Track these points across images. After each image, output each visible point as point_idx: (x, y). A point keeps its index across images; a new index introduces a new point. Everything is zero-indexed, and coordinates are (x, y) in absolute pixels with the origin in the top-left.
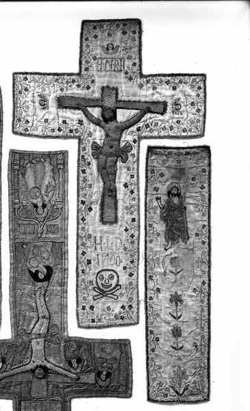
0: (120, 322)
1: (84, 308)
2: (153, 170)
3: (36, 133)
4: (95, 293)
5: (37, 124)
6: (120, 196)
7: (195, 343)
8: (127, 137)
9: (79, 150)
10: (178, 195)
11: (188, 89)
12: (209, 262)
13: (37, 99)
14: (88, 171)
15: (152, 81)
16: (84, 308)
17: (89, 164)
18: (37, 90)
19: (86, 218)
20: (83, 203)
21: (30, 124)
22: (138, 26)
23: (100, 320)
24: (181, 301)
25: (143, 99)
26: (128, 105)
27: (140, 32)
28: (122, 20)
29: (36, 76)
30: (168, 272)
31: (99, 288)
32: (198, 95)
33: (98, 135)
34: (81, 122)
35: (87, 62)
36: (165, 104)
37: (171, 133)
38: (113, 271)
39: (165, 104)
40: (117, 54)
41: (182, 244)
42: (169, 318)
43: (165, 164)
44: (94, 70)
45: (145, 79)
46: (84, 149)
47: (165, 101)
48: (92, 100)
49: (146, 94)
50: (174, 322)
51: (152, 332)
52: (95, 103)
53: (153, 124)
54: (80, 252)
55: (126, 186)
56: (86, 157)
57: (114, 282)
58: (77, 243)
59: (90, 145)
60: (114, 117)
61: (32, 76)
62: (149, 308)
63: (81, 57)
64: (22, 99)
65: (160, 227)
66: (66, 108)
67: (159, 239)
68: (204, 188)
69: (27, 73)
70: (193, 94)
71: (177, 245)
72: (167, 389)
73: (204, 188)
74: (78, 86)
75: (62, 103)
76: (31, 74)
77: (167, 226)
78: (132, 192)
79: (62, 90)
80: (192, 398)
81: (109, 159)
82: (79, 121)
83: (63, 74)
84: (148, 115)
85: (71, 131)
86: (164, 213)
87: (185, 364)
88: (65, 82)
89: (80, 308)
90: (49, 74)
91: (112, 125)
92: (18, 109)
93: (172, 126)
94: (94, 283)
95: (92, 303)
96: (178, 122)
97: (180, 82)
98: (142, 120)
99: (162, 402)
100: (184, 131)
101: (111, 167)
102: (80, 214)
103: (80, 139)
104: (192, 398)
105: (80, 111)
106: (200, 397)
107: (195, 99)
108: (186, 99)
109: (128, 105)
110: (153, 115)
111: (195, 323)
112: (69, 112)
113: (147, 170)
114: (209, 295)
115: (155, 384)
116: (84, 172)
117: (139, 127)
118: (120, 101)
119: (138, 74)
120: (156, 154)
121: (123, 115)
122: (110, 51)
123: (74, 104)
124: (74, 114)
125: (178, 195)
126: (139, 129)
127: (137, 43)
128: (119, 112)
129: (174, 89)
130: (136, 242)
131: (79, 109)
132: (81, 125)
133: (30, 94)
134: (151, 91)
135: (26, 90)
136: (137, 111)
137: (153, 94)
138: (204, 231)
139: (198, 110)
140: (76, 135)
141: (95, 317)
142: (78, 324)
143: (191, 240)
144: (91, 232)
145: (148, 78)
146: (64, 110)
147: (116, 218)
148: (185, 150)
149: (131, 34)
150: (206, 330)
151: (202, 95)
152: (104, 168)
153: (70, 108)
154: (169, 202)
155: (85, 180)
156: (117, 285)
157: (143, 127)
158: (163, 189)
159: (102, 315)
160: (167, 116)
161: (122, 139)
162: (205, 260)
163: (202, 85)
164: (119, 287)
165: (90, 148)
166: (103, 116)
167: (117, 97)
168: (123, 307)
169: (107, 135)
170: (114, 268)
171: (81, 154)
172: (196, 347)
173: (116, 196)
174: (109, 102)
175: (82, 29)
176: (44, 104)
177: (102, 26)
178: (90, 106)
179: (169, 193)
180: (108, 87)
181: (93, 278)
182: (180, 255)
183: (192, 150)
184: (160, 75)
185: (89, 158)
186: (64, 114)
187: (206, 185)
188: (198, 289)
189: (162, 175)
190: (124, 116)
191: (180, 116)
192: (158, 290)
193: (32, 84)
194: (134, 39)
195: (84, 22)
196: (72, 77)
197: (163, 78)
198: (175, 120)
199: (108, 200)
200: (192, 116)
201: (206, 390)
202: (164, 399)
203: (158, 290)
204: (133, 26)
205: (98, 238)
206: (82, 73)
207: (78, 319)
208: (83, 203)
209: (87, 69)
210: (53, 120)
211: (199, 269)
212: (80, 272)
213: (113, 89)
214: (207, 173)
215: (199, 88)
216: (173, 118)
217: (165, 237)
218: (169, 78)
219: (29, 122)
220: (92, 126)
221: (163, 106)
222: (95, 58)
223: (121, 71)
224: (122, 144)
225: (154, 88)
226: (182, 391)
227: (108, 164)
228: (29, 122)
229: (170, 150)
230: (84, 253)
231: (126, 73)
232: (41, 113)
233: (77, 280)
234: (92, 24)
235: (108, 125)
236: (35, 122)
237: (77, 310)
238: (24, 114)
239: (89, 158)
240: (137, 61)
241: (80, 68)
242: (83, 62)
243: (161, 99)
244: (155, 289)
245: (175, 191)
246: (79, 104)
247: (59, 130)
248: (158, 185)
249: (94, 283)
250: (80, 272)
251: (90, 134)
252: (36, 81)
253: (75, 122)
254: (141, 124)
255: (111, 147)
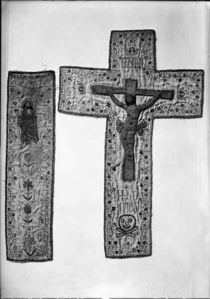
0: (137, 253)
1: (110, 243)
2: (13, 89)
3: (75, 111)
4: (118, 232)
5: (76, 105)
6: (137, 160)
7: (41, 217)
8: (143, 116)
9: (107, 125)
10: (31, 108)
11: (189, 81)
12: (54, 157)
13: (77, 86)
14: (113, 141)
15: (163, 75)
16: (110, 243)
17: (114, 135)
18: (77, 80)
19: (111, 176)
20: (109, 164)
21: (71, 105)
22: (153, 35)
23: (121, 252)
24: (32, 187)
25: (156, 89)
26: (144, 93)
27: (155, 39)
28: (141, 30)
29: (77, 70)
30: (22, 164)
31: (121, 229)
32: (197, 86)
33: (122, 115)
34: (109, 105)
35: (114, 61)
36: (172, 92)
37: (177, 114)
38: (132, 216)
39: (172, 92)
40: (137, 55)
41: (33, 143)
42: (23, 200)
43: (21, 84)
44: (120, 68)
45: (158, 74)
46: (111, 125)
47: (173, 90)
48: (118, 89)
49: (159, 85)
50: (26, 202)
51: (9, 209)
52: (120, 91)
53: (164, 107)
54: (107, 201)
55: (141, 153)
56: (112, 130)
57: (132, 224)
58: (105, 194)
59: (115, 122)
60: (134, 102)
61: (74, 69)
62: (8, 192)
63: (110, 57)
64: (66, 86)
65: (17, 131)
66: (98, 94)
67: (17, 140)
68: (50, 102)
69: (70, 67)
70: (194, 84)
71: (29, 145)
72: (21, 252)
73: (50, 102)
74: (108, 78)
75: (95, 90)
76: (73, 67)
77: (22, 131)
78: (146, 157)
79: (95, 80)
80: (40, 258)
81: (129, 133)
82: (108, 104)
83: (97, 69)
84: (160, 101)
85: (101, 111)
86: (21, 121)
87: (33, 233)
88: (98, 75)
89: (107, 242)
90: (87, 69)
91: (132, 108)
92: (63, 93)
93: (177, 109)
94: (117, 224)
95: (116, 239)
96: (182, 105)
97: (184, 76)
98: (155, 104)
99: (17, 261)
100: (187, 112)
101: (130, 138)
102: (107, 172)
103: (108, 120)
104: (40, 258)
105: (109, 97)
106: (45, 258)
107: (194, 88)
108: (189, 88)
109: (144, 93)
110: (163, 100)
111: (42, 202)
112: (100, 97)
113: (8, 89)
114: (53, 182)
115: (12, 247)
116: (110, 141)
117: (153, 109)
118: (139, 90)
119: (152, 70)
120: (14, 77)
121: (140, 101)
122: (132, 53)
123: (104, 91)
124: (104, 98)
125: (31, 108)
126: (152, 111)
127: (151, 47)
128: (138, 98)
129: (180, 80)
130: (149, 195)
131: (108, 95)
132: (109, 106)
133: (72, 82)
134: (162, 83)
135: (69, 79)
136: (151, 97)
137: (164, 85)
138: (49, 134)
139: (197, 97)
140: (105, 114)
141: (118, 250)
142: (106, 255)
143: (40, 141)
144: (115, 187)
145: (160, 73)
146: (97, 95)
147: (134, 176)
148: (36, 74)
149: (148, 41)
150: (49, 207)
151: (200, 86)
152: (125, 139)
153: (101, 94)
154: (24, 112)
155: (111, 148)
156: (135, 226)
157: (156, 109)
158: (19, 104)
159: (123, 248)
160: (174, 101)
161: (140, 118)
162: (50, 156)
163: (200, 78)
164: (136, 228)
165: (115, 124)
166: (126, 101)
167: (136, 87)
168: (139, 243)
169: (129, 115)
170: (132, 213)
171: (109, 128)
172: (42, 220)
173: (134, 160)
174: (131, 90)
175: (111, 37)
176: (82, 90)
177: (125, 35)
178: (116, 93)
179: (24, 106)
180: (130, 79)
181: (115, 221)
182: (32, 152)
183: (41, 74)
184: (169, 71)
185: (114, 132)
186: (97, 99)
187: (51, 100)
188: (44, 177)
189: (19, 93)
190: (141, 101)
191: (184, 101)
192: (15, 178)
193: (74, 75)
194: (149, 44)
195: (113, 32)
196: (104, 72)
197: (172, 73)
198: (179, 104)
199: (129, 164)
200: (193, 101)
201: (49, 252)
202: (19, 259)
203: (15, 178)
204: (149, 36)
205: (120, 192)
206: (111, 69)
207: (105, 251)
208: (109, 164)
209: (114, 66)
210: (89, 102)
211: (45, 162)
212: (107, 216)
213: (134, 81)
214: (52, 91)
215: (198, 80)
216: (178, 102)
217: (21, 139)
218: (177, 73)
219: (70, 103)
220: (117, 108)
221: (171, 94)
222: (120, 58)
223: (140, 67)
224: (139, 123)
225: (165, 80)
226: (32, 252)
227: (128, 137)
228: (70, 103)
229: (25, 74)
230: (110, 202)
231: (144, 69)
232: (79, 96)
233: (105, 223)
234: (118, 33)
235: (129, 108)
236: (75, 103)
237: (105, 245)
238: (67, 97)
239: (114, 132)
240: (152, 60)
241: (110, 65)
242: (112, 61)
243: (169, 88)
244: (13, 177)
245: (28, 105)
246: (109, 92)
247: (93, 110)
248: (17, 101)
249: (117, 224)
250: (107, 216)
251: (116, 114)
252: (76, 73)
253: (104, 105)
254: (154, 107)
255: (131, 124)
